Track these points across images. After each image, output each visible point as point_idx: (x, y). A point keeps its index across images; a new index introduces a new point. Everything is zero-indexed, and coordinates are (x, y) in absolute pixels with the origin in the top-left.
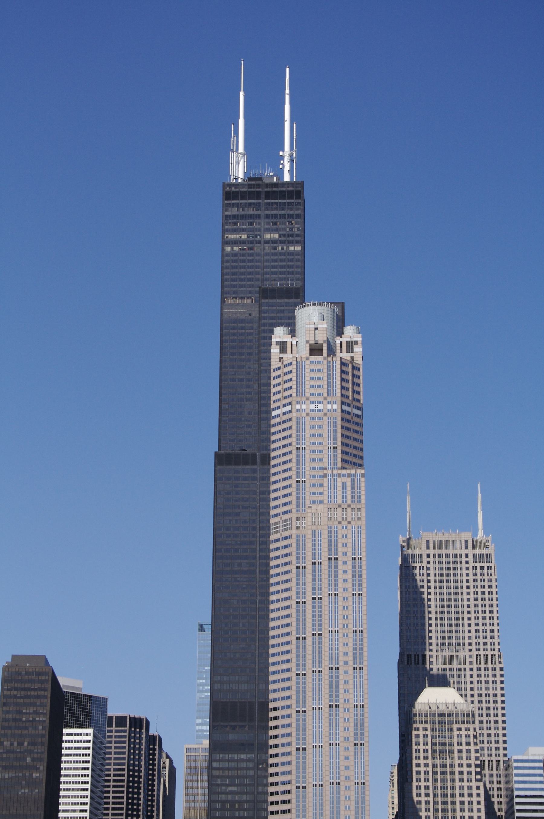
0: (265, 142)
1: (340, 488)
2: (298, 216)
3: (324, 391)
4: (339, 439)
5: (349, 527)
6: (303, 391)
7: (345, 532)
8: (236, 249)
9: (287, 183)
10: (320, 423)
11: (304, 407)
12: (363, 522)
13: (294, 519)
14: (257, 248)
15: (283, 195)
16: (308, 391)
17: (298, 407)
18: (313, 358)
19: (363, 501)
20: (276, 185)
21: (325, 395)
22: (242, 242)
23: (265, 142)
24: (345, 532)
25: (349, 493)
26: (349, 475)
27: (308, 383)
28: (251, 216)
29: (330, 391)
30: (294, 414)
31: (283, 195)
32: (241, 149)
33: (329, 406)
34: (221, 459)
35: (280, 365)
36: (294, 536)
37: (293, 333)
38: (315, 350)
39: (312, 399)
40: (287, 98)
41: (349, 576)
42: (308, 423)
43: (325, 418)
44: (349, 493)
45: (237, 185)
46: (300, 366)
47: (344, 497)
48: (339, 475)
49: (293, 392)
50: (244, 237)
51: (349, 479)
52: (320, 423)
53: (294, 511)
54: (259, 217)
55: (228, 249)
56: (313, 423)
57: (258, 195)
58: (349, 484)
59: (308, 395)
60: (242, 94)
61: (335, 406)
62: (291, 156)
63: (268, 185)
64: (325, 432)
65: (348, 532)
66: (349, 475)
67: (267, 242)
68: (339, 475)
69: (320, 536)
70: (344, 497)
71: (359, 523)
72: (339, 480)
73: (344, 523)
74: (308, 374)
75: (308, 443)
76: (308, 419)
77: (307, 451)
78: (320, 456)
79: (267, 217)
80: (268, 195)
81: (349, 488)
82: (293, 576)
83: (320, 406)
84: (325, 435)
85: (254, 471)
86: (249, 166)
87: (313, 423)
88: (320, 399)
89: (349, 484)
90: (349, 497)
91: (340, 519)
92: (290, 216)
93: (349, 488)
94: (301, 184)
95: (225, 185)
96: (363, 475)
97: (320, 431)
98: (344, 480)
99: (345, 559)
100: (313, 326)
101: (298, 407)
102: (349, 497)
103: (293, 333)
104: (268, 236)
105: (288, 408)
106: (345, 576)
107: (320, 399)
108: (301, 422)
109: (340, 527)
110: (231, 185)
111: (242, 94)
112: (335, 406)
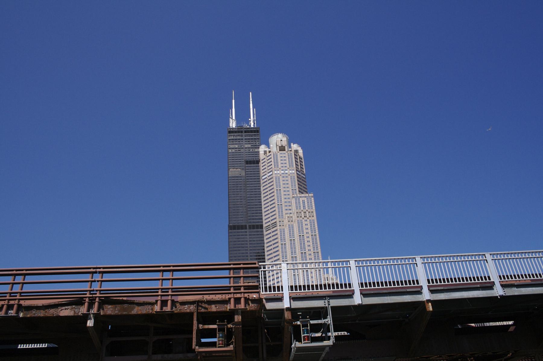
0: (243, 115)
1: (301, 203)
2: (258, 139)
3: (288, 165)
4: (297, 185)
5: (308, 220)
6: (278, 166)
7: (306, 223)
8: (233, 151)
9: (252, 128)
10: (287, 179)
11: (278, 172)
12: (315, 218)
13: (278, 222)
14: (242, 150)
15: (251, 132)
16: (280, 166)
17: (276, 172)
18: (281, 152)
19: (314, 208)
20: (249, 128)
21: (288, 167)
22: (236, 148)
23: (243, 115)
24: (306, 223)
25: (306, 204)
26: (305, 197)
27: (280, 162)
28: (239, 139)
29: (291, 165)
30: (274, 175)
31: (251, 132)
32: (234, 118)
33: (291, 172)
34: (231, 228)
35: (265, 156)
36: (279, 230)
37: (269, 147)
38: (282, 149)
39: (282, 169)
40: (251, 102)
41: (311, 243)
42: (281, 179)
43: (289, 177)
44: (306, 204)
45: (233, 129)
46: (275, 156)
47: (304, 207)
48: (301, 197)
49: (273, 166)
50: (237, 146)
51: (306, 199)
52: (287, 179)
53: (278, 218)
54: (242, 139)
55: (230, 151)
56: (284, 179)
57: (242, 132)
58: (306, 201)
59: (280, 167)
60: (233, 101)
61: (293, 172)
62: (254, 121)
63: (245, 128)
64: (290, 182)
65: (308, 222)
66: (305, 197)
67: (246, 148)
68: (301, 197)
69: (293, 227)
70: (304, 207)
71: (313, 218)
72: (301, 199)
73: (305, 218)
74: (279, 159)
75: (282, 188)
76: (281, 177)
77: (282, 191)
78: (288, 193)
79: (246, 139)
80: (245, 132)
81: (306, 203)
82: (280, 248)
83: (286, 172)
84: (290, 184)
85: (246, 232)
86: (237, 123)
87: (284, 179)
88: (286, 168)
89: (306, 201)
90: (306, 206)
91: (303, 217)
92: (255, 139)
93: (306, 203)
94: (259, 128)
95: (228, 129)
96: (312, 197)
97: (287, 182)
98: (303, 199)
99: (308, 235)
100: (280, 139)
101: (276, 172)
102: (306, 206)
103: (269, 147)
104: (246, 146)
105: (271, 173)
106: (309, 244)
107: (286, 168)
108: (278, 179)
109: (303, 220)
110: (231, 129)
111: (233, 101)
112: (293, 172)
